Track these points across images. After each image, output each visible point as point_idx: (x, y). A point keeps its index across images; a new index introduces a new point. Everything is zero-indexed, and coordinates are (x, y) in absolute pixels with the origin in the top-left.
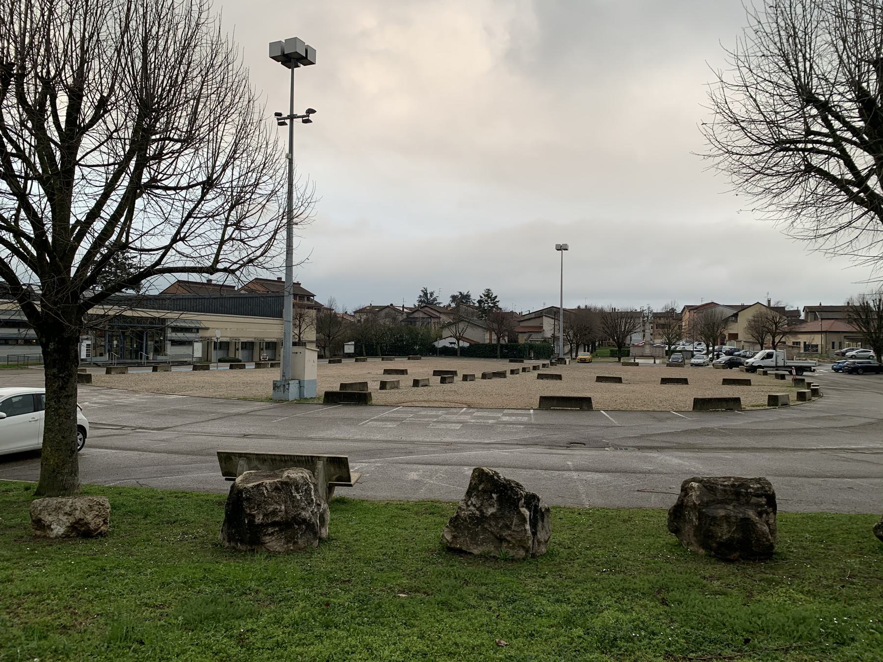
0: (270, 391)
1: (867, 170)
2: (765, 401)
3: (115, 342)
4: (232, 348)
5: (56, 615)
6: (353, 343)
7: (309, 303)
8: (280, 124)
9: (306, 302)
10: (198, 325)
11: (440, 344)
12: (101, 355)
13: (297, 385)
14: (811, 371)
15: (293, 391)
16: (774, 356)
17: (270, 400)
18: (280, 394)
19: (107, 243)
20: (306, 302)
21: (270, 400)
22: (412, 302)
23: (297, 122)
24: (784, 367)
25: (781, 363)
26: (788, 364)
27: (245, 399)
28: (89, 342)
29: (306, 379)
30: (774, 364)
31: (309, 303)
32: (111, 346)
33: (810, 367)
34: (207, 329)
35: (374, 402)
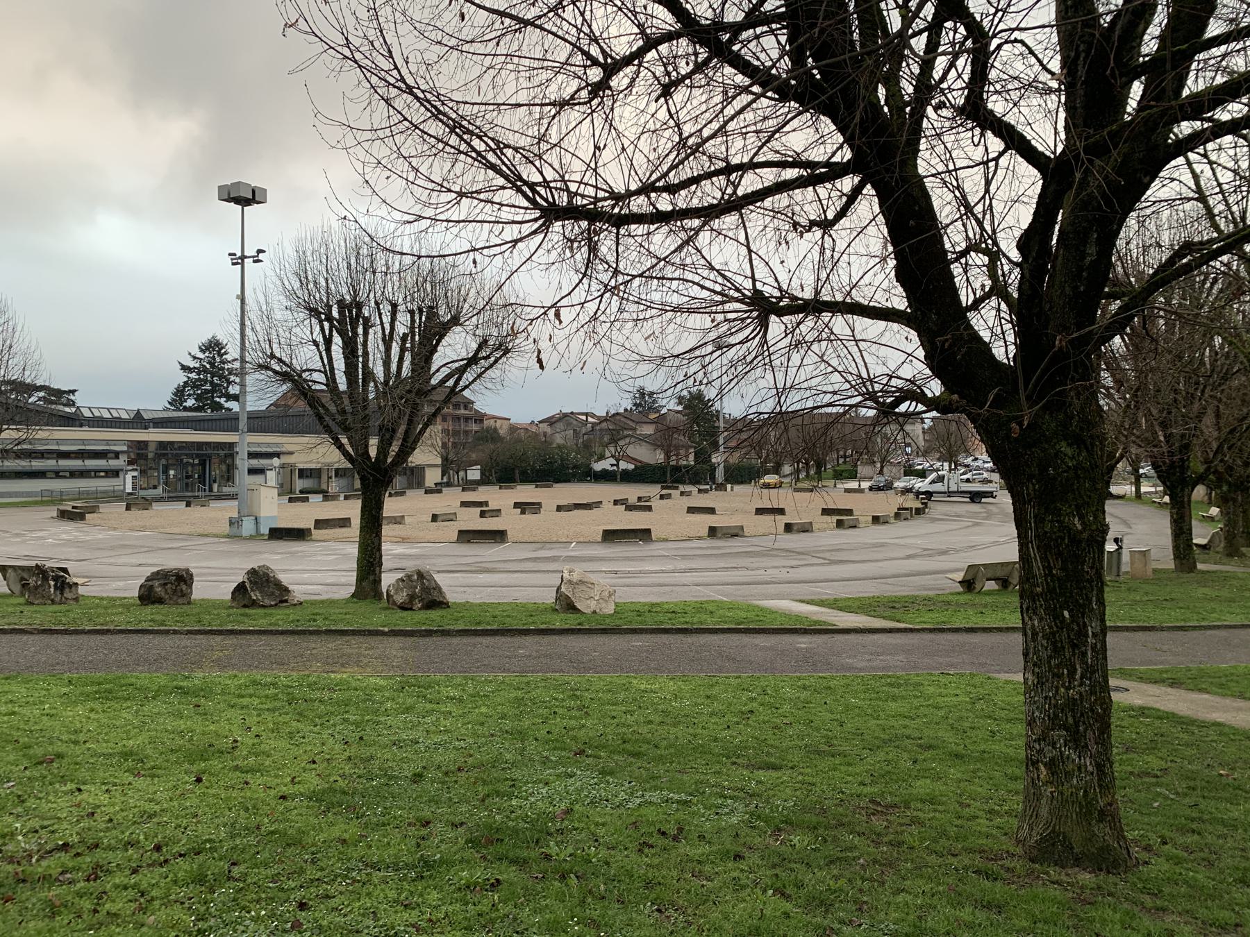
0: (226, 529)
1: (462, 363)
2: (705, 532)
3: (172, 472)
4: (324, 477)
5: (238, 841)
6: (479, 467)
7: (467, 412)
8: (234, 264)
9: (462, 411)
10: (278, 450)
11: (598, 466)
12: (155, 487)
13: (253, 522)
14: (992, 497)
15: (248, 527)
16: (946, 481)
17: (228, 536)
18: (235, 530)
19: (933, 102)
20: (462, 411)
21: (228, 536)
22: (626, 403)
23: (248, 262)
24: (958, 492)
25: (953, 488)
26: (963, 489)
27: (203, 535)
28: (135, 474)
29: (262, 515)
30: (944, 489)
31: (467, 412)
32: (168, 476)
33: (992, 492)
34: (291, 453)
35: (313, 537)
